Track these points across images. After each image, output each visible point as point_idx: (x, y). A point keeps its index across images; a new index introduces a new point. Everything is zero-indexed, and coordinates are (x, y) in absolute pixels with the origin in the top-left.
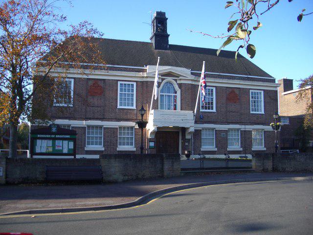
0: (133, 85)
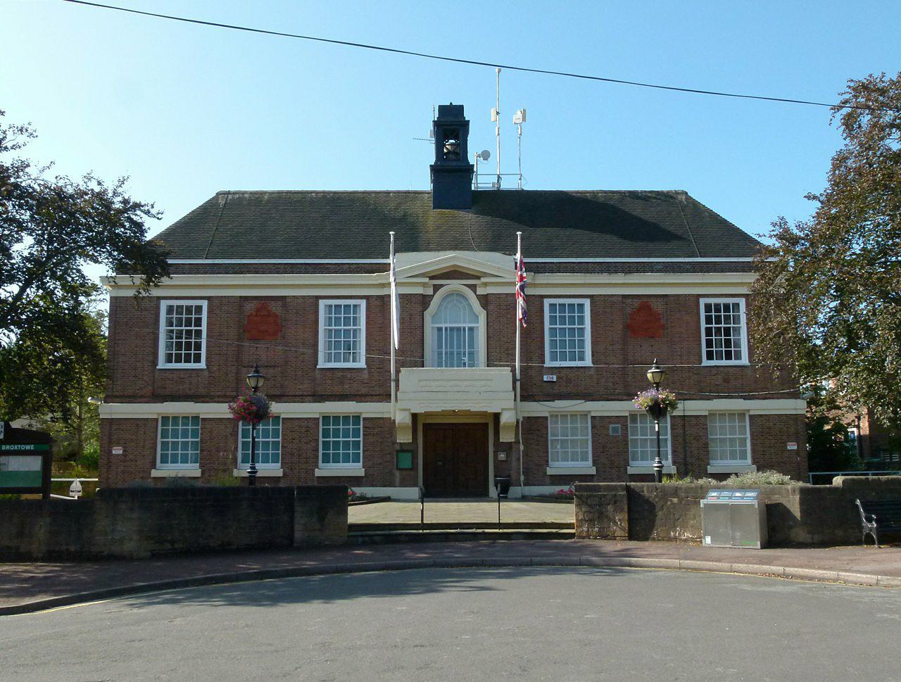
0: (581, 306)
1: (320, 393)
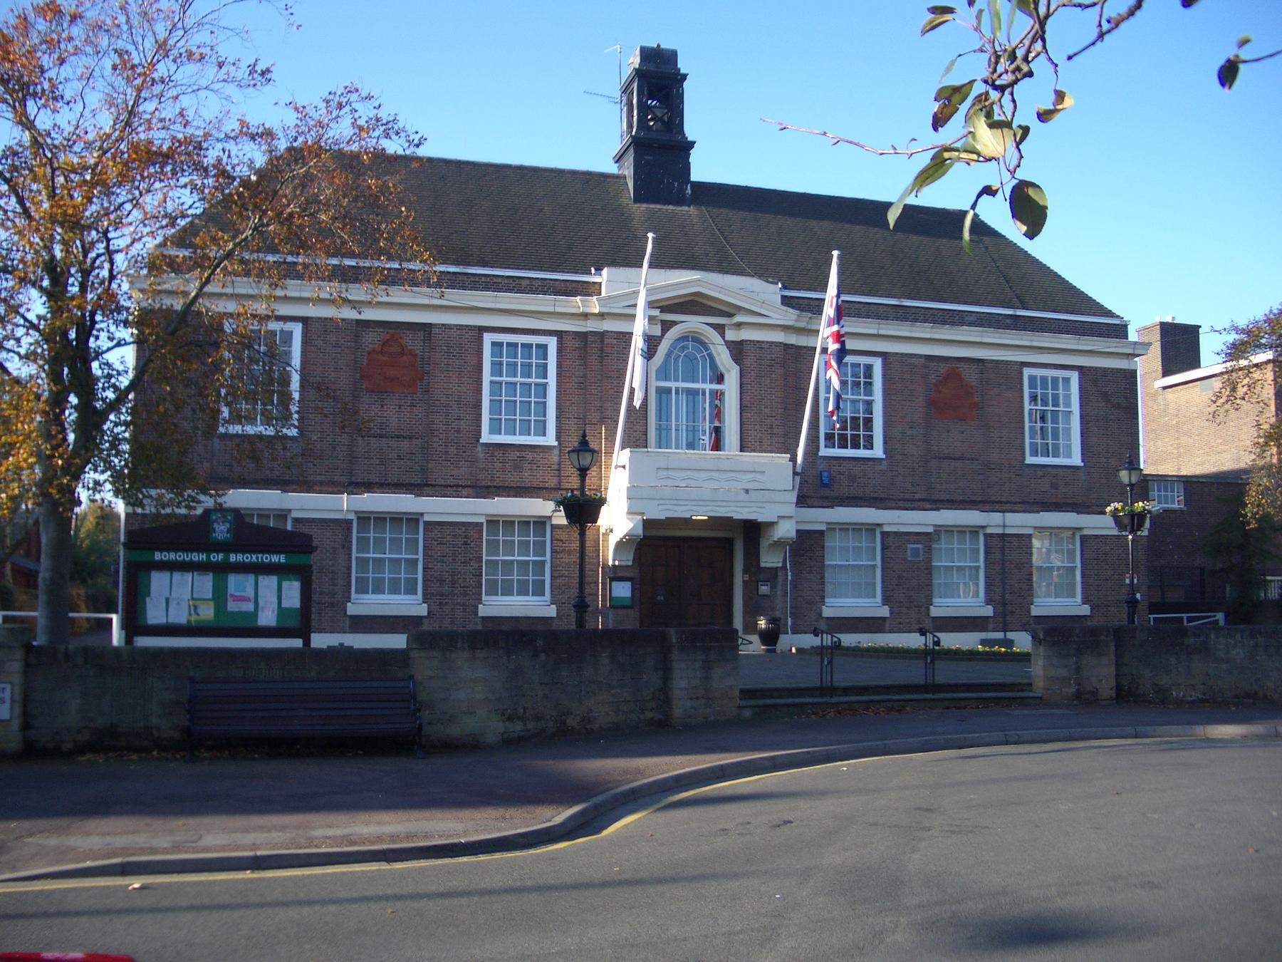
0: (543, 348)
1: (484, 484)
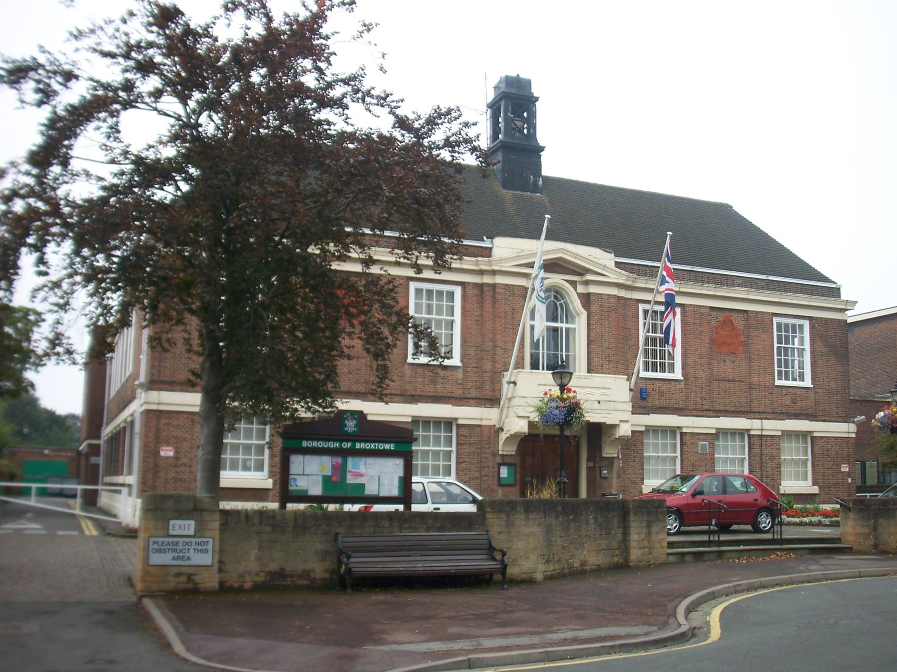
0: (451, 295)
1: (409, 393)
